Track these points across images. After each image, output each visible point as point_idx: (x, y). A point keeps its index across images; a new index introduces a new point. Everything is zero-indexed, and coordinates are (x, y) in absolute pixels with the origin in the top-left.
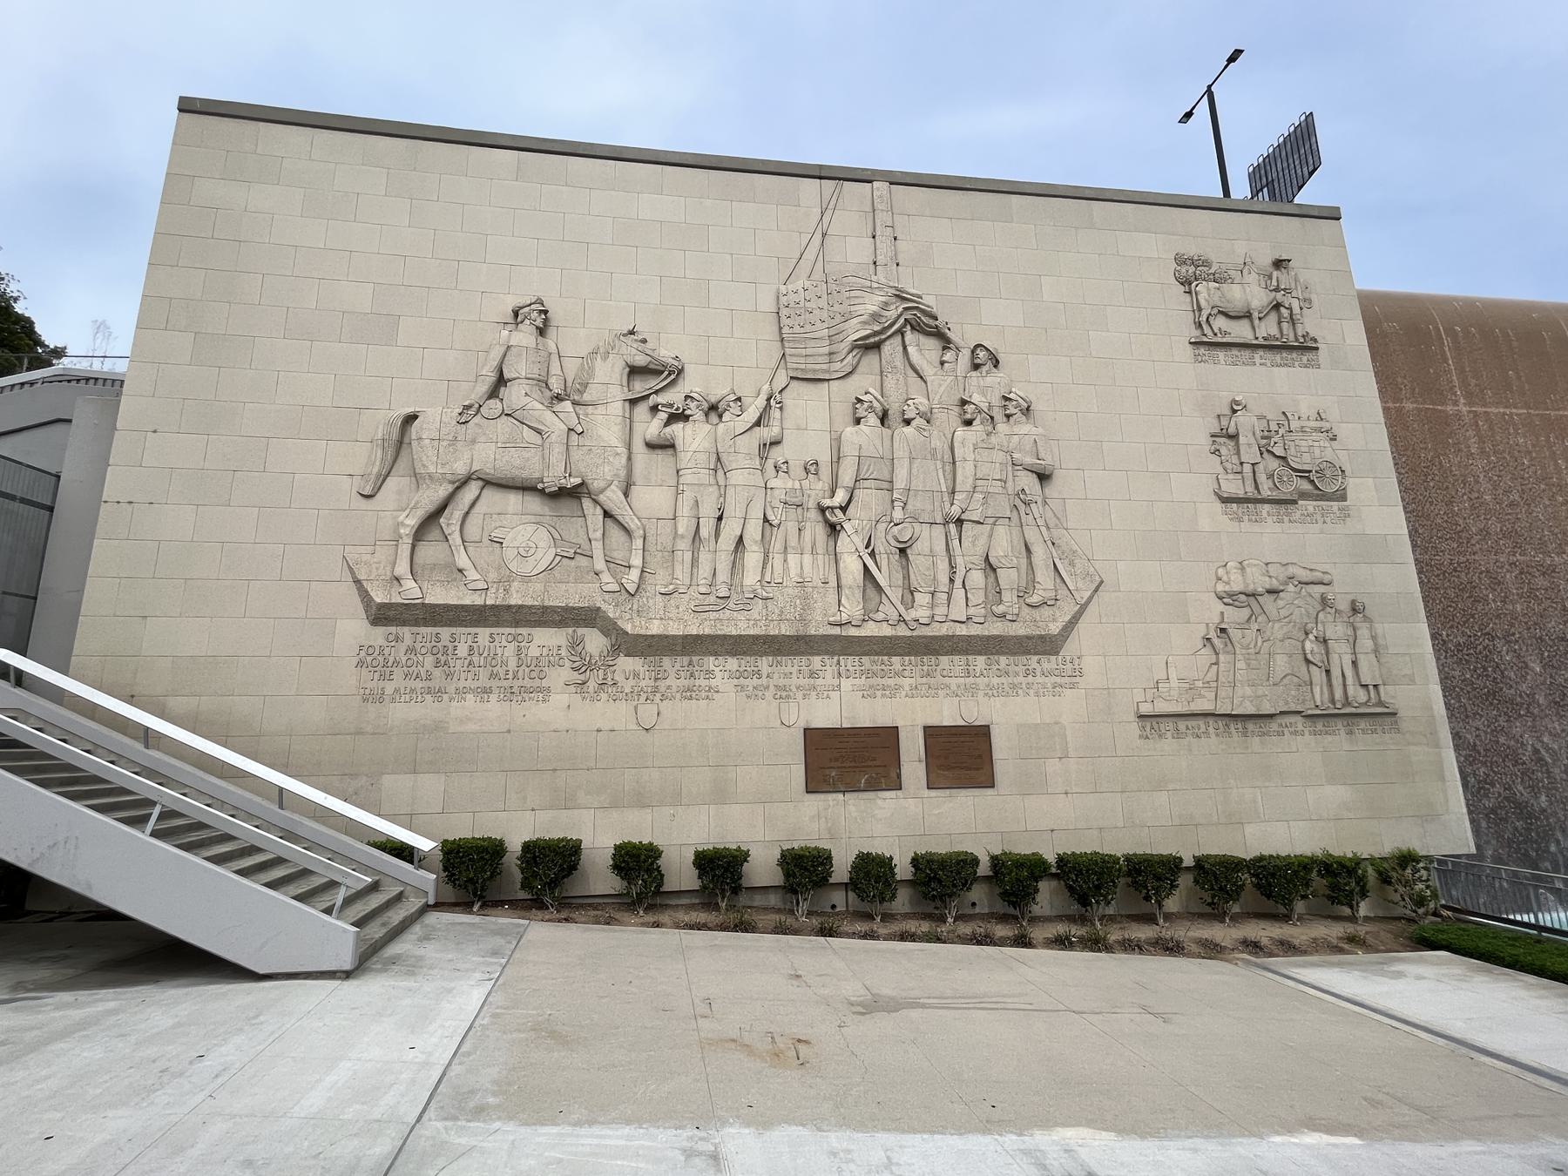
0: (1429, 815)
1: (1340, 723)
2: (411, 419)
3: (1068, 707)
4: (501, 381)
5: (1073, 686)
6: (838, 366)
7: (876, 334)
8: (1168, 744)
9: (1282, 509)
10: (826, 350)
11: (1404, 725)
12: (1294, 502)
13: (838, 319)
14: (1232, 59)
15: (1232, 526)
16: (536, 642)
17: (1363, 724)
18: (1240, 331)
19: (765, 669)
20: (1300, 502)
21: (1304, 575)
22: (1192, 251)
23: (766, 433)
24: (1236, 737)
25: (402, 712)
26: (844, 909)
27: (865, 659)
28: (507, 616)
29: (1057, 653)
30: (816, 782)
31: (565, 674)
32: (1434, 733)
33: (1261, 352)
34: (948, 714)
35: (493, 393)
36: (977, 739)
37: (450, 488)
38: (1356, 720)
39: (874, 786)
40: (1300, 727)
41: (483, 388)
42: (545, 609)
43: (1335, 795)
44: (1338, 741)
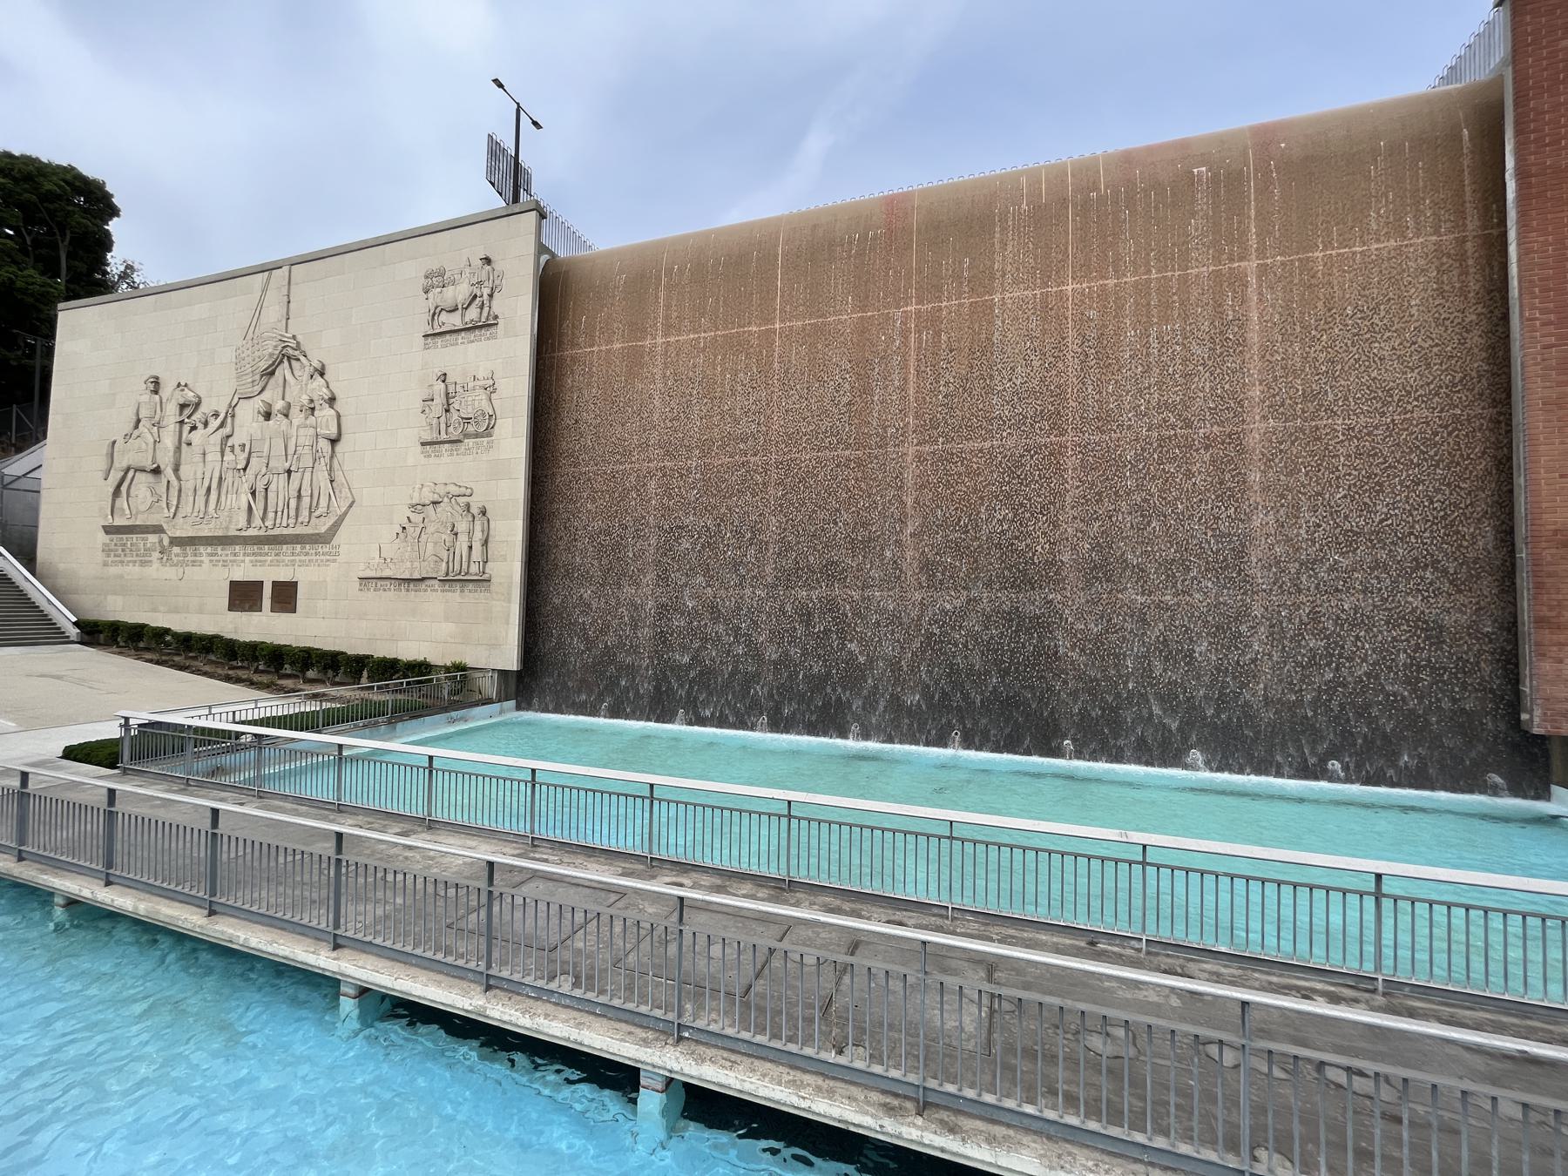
0: (494, 645)
1: (458, 585)
2: (114, 442)
3: (330, 573)
4: (139, 421)
5: (334, 561)
6: (255, 388)
7: (270, 366)
8: (371, 594)
9: (454, 446)
10: (250, 380)
11: (492, 588)
12: (460, 441)
13: (257, 360)
14: (501, 86)
15: (423, 460)
16: (150, 540)
17: (471, 586)
18: (454, 320)
19: (220, 552)
20: (466, 441)
21: (454, 490)
22: (435, 266)
23: (227, 430)
24: (403, 592)
25: (113, 570)
26: (957, 1024)
27: (255, 547)
28: (215, 542)
29: (329, 543)
30: (232, 606)
31: (156, 555)
32: (509, 594)
33: (463, 334)
34: (284, 575)
35: (136, 427)
36: (292, 586)
37: (122, 473)
38: (467, 584)
39: (251, 609)
40: (436, 587)
41: (132, 425)
42: (147, 526)
43: (448, 628)
44: (455, 596)
